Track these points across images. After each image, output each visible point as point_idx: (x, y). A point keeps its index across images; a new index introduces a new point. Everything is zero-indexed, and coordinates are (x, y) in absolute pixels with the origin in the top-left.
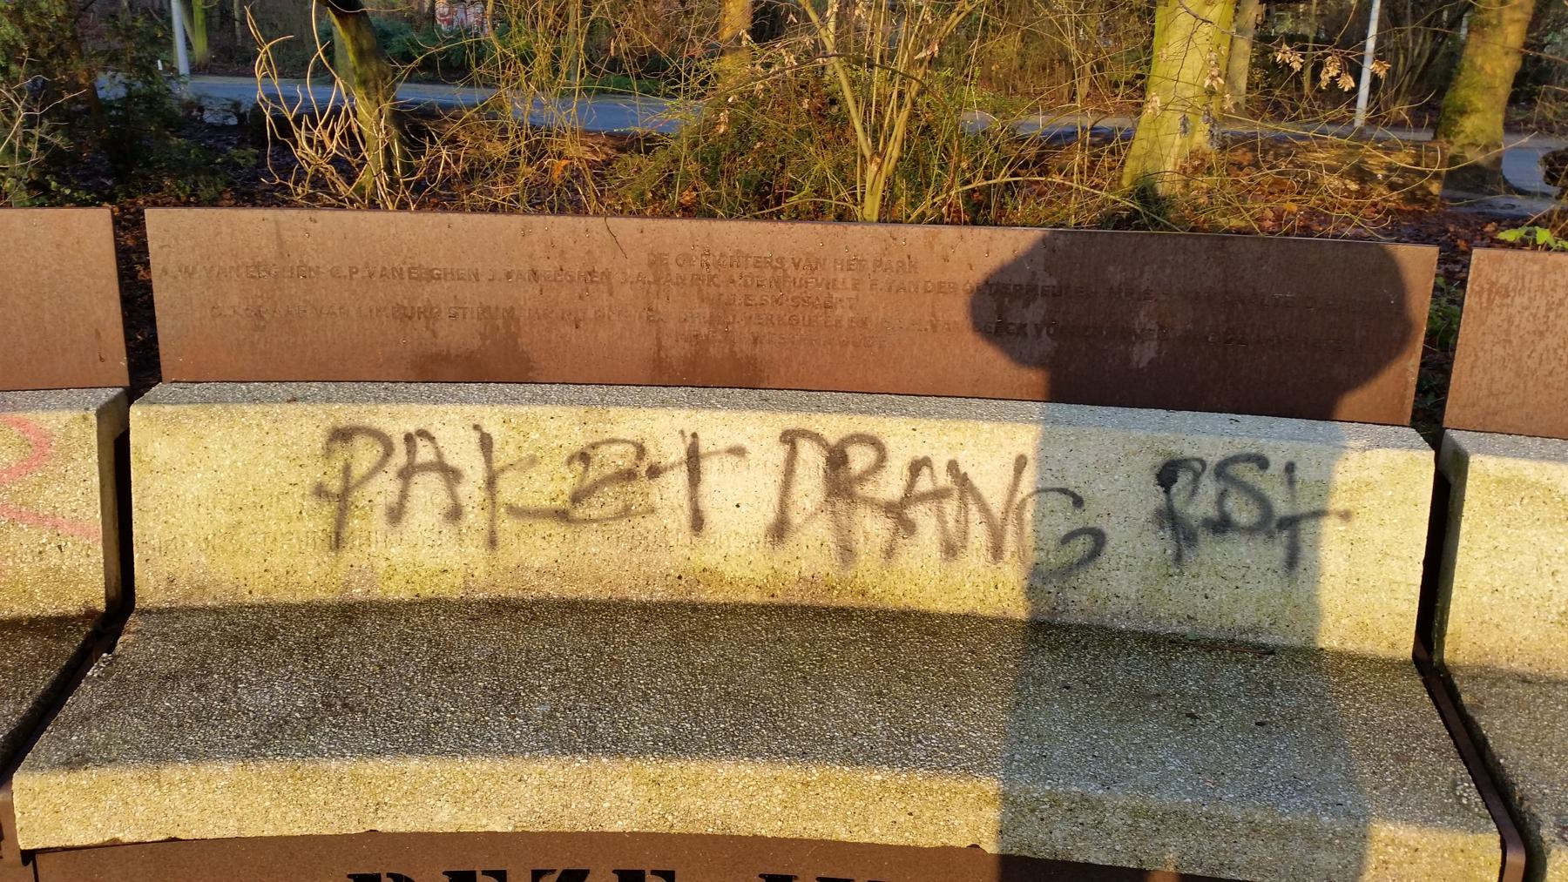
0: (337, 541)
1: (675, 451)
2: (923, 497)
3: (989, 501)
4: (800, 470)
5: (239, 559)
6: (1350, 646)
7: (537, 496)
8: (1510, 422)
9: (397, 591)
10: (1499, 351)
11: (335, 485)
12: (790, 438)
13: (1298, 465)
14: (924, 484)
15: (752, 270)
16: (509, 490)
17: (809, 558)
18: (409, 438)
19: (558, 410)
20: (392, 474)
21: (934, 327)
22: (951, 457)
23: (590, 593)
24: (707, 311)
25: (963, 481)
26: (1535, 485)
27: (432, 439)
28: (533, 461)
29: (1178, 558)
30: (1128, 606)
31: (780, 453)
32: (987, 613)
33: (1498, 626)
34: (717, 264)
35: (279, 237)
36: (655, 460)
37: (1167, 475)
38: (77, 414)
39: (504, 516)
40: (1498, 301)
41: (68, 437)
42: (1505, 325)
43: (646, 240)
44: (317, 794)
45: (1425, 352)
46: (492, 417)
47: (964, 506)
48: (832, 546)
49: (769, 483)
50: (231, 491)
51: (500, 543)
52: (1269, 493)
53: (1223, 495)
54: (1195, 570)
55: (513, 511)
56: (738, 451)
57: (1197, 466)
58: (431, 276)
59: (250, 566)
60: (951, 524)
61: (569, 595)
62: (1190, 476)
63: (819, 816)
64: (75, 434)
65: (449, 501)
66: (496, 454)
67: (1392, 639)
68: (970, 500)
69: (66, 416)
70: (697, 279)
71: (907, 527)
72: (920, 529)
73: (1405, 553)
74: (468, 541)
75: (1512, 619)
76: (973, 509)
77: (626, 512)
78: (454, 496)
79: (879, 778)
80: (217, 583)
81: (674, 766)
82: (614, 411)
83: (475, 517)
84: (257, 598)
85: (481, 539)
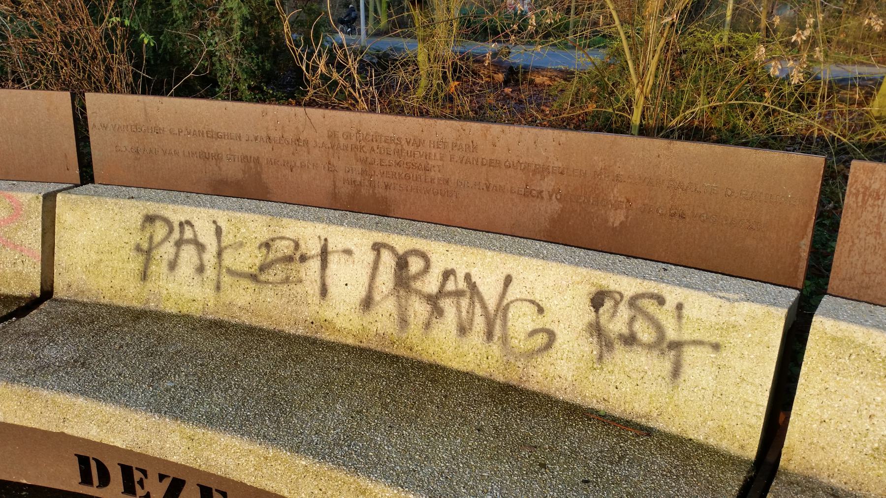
0: (144, 276)
1: (314, 248)
2: (450, 294)
3: (487, 302)
4: (381, 268)
5: (100, 279)
6: (712, 441)
7: (242, 265)
8: (879, 295)
9: (170, 308)
10: (871, 240)
11: (145, 246)
12: (377, 247)
13: (685, 305)
14: (450, 286)
15: (383, 144)
16: (228, 259)
17: (382, 323)
18: (181, 224)
19: (256, 217)
20: (172, 243)
21: (488, 188)
22: (467, 271)
23: (265, 325)
24: (359, 167)
25: (473, 287)
26: (862, 346)
27: (192, 226)
28: (241, 245)
29: (601, 358)
30: (566, 385)
31: (371, 256)
32: (481, 374)
33: (823, 448)
34: (365, 139)
35: (145, 111)
36: (304, 251)
37: (597, 300)
38: (34, 195)
39: (225, 274)
40: (870, 202)
41: (29, 206)
42: (876, 221)
43: (326, 123)
44: (37, 407)
45: (814, 236)
46: (222, 217)
47: (472, 303)
48: (396, 317)
49: (364, 274)
50: (99, 243)
51: (222, 289)
52: (664, 323)
53: (632, 320)
54: (611, 368)
55: (230, 272)
56: (348, 252)
57: (618, 297)
58: (218, 136)
59: (104, 284)
60: (464, 314)
61: (254, 324)
62: (612, 303)
63: (274, 480)
64: (33, 205)
65: (198, 261)
66: (223, 238)
67: (742, 442)
68: (476, 300)
69: (30, 196)
70: (354, 148)
71: (438, 312)
72: (446, 314)
73: (757, 381)
74: (206, 286)
75: (835, 446)
76: (478, 305)
77: (286, 280)
78: (201, 259)
79: (304, 463)
80: (90, 290)
81: (200, 431)
82: (285, 221)
83: (210, 273)
84: (106, 301)
85: (213, 285)
